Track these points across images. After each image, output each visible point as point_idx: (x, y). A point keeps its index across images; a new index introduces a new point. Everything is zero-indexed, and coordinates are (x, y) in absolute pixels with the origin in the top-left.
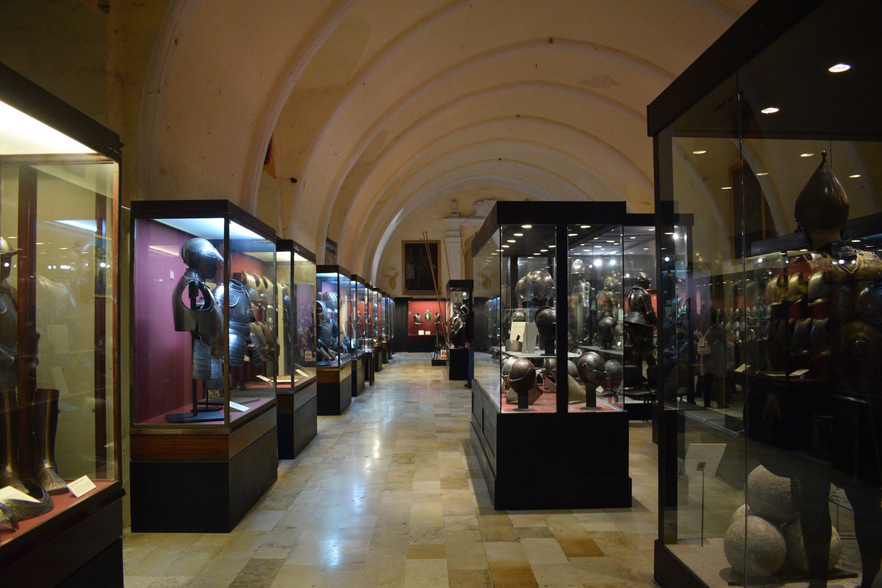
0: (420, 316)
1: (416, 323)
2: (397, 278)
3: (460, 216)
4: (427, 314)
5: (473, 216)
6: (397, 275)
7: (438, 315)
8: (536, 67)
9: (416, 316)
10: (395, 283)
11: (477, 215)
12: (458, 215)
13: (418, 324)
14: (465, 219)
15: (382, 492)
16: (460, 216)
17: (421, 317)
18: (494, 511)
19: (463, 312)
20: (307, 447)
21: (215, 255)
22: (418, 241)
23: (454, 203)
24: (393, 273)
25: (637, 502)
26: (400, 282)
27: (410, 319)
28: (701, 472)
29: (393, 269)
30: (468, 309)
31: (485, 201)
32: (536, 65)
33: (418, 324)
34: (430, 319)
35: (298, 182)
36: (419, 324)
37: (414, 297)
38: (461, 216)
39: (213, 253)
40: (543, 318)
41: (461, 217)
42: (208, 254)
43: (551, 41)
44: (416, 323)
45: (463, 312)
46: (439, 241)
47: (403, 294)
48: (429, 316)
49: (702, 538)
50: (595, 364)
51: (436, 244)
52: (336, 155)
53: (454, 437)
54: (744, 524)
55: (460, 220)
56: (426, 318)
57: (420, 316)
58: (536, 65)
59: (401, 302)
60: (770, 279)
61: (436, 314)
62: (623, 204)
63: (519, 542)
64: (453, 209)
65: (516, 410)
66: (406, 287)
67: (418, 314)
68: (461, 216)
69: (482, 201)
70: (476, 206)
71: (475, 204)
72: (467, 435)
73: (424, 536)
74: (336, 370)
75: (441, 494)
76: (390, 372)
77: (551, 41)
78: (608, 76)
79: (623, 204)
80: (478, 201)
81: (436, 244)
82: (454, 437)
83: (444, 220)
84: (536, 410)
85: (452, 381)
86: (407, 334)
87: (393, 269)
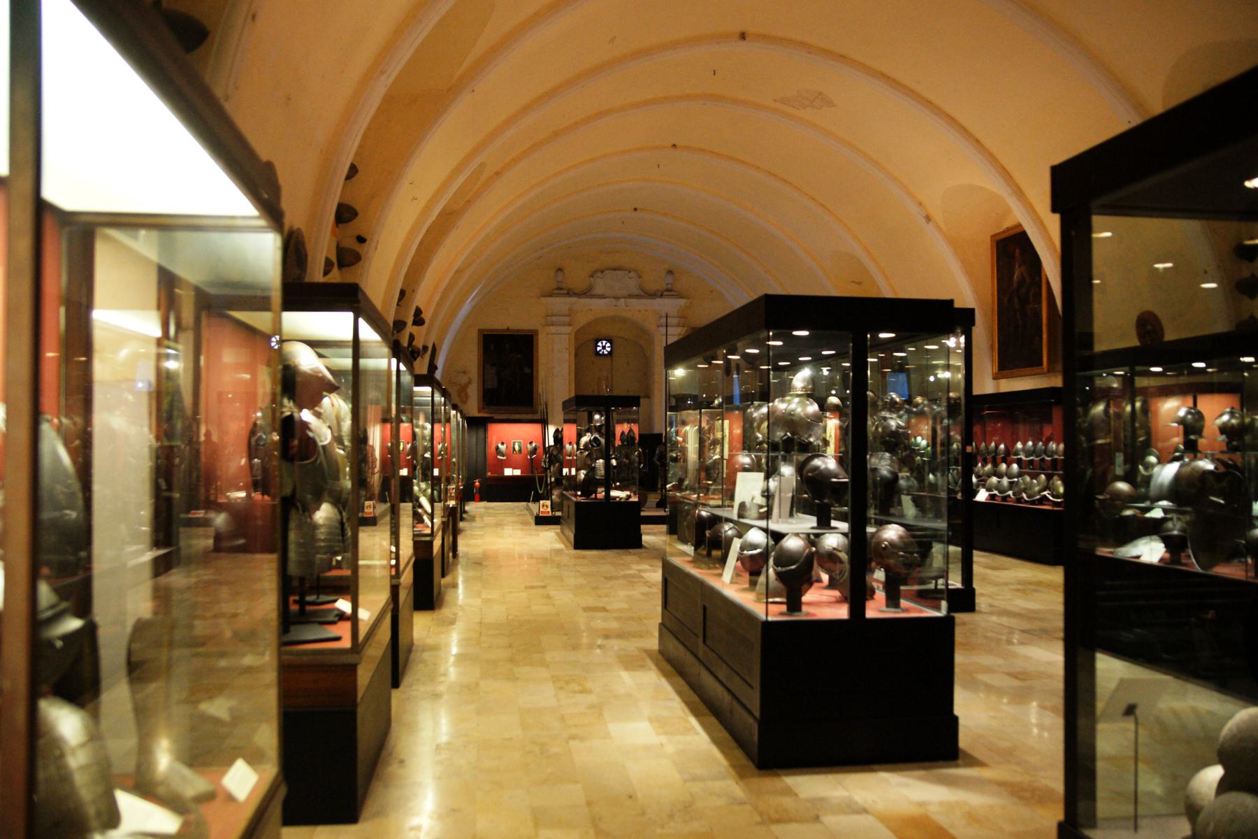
0: (505, 445)
1: (499, 457)
2: (470, 386)
3: (568, 293)
4: (517, 444)
5: (589, 294)
6: (470, 382)
7: (534, 445)
8: (715, 74)
9: (500, 445)
10: (467, 397)
11: (593, 293)
12: (565, 292)
13: (502, 458)
14: (576, 299)
15: (567, 742)
16: (568, 293)
17: (507, 447)
18: (756, 771)
19: (595, 444)
20: (407, 667)
21: (321, 372)
22: (503, 330)
23: (560, 273)
24: (463, 379)
25: (964, 752)
26: (474, 393)
27: (492, 450)
28: (1132, 718)
29: (464, 372)
30: (603, 441)
31: (607, 272)
32: (714, 71)
33: (502, 458)
34: (520, 451)
35: (367, 242)
36: (505, 458)
37: (497, 417)
38: (570, 293)
39: (317, 368)
40: (817, 472)
41: (570, 296)
42: (311, 370)
43: (743, 36)
44: (499, 457)
45: (595, 444)
46: (536, 332)
47: (479, 412)
48: (519, 446)
49: (1136, 817)
50: (901, 545)
51: (532, 336)
52: (416, 199)
53: (633, 646)
54: (1132, 787)
55: (569, 300)
56: (514, 449)
57: (505, 445)
58: (714, 71)
59: (476, 424)
60: (1093, 405)
61: (531, 443)
62: (951, 302)
63: (821, 822)
64: (558, 282)
65: (782, 614)
66: (483, 401)
67: (503, 444)
68: (570, 293)
69: (602, 272)
70: (592, 279)
71: (592, 276)
72: (653, 643)
73: (671, 816)
74: (428, 539)
75: (662, 744)
76: (474, 535)
77: (743, 36)
78: (820, 94)
79: (951, 302)
80: (596, 272)
81: (532, 336)
82: (633, 646)
83: (543, 300)
84: (814, 615)
85: (579, 552)
86: (485, 472)
87: (464, 372)
